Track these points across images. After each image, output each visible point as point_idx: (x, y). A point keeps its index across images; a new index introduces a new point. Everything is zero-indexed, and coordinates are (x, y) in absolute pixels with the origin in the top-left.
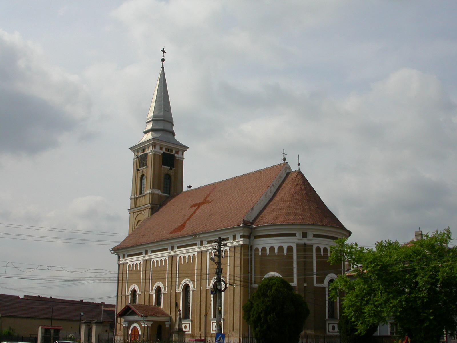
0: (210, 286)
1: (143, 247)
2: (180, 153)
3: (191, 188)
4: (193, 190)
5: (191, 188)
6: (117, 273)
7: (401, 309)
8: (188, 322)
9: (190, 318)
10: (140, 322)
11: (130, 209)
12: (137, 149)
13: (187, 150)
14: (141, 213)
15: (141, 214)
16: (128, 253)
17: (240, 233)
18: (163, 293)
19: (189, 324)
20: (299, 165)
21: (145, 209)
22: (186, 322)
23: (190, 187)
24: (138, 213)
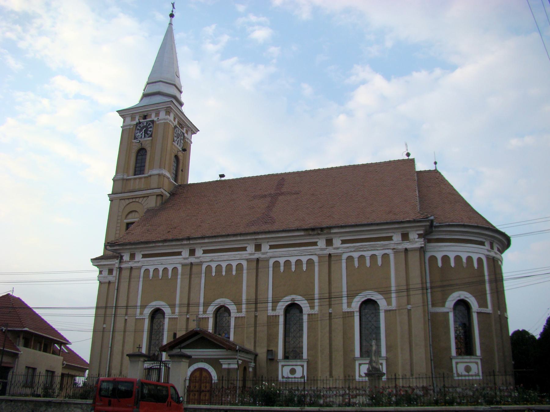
0: (351, 307)
1: (217, 240)
2: (190, 133)
3: (223, 179)
4: (225, 181)
5: (223, 179)
6: (189, 274)
7: (257, 388)
8: (299, 363)
9: (305, 356)
10: (220, 360)
11: (111, 193)
12: (132, 114)
13: (196, 134)
14: (140, 201)
15: (142, 204)
16: (143, 251)
17: (417, 230)
18: (236, 318)
19: (302, 366)
20: (435, 163)
21: (148, 196)
22: (294, 363)
23: (222, 176)
24: (131, 201)
